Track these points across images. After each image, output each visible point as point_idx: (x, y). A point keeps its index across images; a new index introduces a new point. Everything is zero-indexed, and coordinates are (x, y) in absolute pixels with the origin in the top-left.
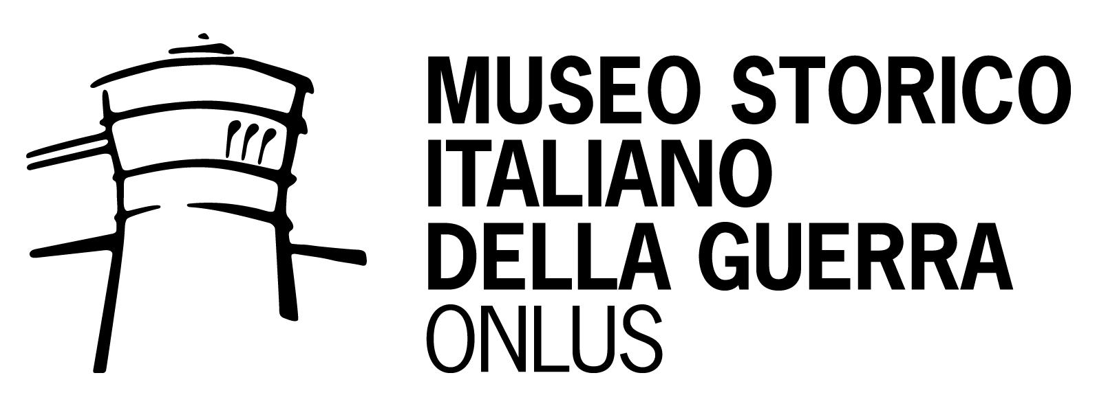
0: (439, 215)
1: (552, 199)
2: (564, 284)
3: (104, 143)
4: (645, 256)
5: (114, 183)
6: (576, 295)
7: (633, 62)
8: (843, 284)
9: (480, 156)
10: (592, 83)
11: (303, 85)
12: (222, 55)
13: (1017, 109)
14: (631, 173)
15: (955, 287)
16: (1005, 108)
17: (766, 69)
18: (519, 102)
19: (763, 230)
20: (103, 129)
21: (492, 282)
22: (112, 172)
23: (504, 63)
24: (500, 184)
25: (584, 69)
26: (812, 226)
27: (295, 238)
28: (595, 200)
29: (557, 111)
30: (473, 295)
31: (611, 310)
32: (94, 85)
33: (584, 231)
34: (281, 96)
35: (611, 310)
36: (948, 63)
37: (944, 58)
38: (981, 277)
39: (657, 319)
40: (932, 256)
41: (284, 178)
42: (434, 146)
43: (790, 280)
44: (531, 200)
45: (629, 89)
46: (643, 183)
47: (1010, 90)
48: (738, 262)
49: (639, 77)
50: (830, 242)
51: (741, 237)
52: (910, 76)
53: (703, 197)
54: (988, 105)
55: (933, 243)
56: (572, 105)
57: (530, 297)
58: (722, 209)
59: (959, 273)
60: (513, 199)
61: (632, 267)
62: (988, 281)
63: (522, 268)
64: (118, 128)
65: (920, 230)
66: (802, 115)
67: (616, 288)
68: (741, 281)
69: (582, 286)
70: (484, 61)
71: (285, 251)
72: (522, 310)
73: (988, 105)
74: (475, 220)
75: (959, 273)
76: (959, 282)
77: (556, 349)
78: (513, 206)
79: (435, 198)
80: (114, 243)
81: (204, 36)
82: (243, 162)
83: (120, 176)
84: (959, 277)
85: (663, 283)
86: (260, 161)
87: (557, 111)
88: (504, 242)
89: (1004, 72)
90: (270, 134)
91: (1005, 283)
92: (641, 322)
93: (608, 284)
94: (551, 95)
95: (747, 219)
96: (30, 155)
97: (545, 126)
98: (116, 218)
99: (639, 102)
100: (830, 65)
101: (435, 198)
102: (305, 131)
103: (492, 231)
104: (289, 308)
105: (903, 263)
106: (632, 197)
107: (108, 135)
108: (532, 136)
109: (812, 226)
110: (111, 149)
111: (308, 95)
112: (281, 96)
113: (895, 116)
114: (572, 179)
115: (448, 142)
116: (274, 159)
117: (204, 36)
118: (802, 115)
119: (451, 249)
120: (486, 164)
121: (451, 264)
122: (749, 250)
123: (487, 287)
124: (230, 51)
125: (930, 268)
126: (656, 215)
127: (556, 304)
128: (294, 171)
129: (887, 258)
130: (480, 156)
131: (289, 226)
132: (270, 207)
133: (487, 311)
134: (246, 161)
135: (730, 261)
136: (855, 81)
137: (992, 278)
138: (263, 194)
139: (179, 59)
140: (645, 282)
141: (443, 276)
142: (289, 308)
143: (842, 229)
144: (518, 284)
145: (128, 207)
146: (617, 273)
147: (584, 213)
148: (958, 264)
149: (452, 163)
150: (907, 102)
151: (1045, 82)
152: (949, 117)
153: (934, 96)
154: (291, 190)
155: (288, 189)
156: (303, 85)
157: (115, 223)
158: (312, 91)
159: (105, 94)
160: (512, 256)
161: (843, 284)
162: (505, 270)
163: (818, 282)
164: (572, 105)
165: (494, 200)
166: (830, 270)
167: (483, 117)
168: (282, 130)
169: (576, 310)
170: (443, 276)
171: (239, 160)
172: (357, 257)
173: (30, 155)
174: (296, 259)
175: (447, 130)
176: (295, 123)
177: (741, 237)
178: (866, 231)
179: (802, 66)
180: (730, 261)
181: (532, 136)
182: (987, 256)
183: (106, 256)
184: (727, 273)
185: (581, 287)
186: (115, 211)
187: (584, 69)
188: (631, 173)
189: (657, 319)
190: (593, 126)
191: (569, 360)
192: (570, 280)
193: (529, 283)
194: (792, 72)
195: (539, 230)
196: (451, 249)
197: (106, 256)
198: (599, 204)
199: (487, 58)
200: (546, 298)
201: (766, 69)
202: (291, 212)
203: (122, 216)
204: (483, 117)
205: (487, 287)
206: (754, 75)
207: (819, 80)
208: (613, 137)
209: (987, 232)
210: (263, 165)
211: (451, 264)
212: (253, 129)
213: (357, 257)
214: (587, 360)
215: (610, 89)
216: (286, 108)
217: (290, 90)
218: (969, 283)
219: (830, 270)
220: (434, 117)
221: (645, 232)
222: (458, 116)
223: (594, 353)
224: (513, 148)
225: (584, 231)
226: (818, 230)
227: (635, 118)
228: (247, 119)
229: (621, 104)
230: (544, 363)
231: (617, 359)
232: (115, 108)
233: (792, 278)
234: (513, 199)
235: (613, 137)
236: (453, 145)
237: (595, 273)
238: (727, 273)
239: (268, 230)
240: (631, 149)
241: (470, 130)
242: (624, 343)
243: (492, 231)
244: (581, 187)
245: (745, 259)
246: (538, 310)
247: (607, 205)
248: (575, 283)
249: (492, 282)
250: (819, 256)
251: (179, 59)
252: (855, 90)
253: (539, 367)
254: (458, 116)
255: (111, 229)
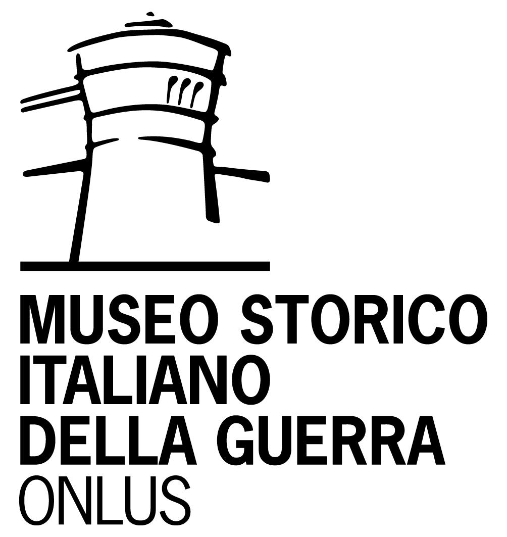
0: (29, 410)
1: (110, 399)
2: (119, 460)
3: (77, 92)
4: (178, 440)
5: (85, 122)
6: (127, 469)
7: (169, 299)
8: (322, 460)
9: (58, 367)
10: (139, 315)
11: (223, 50)
12: (163, 28)
13: (448, 333)
14: (168, 380)
15: (403, 463)
16: (439, 332)
17: (266, 304)
18: (87, 329)
19: (263, 421)
20: (76, 82)
21: (67, 459)
22: (83, 114)
23: (75, 300)
24: (73, 388)
25: (133, 304)
26: (300, 419)
27: (217, 162)
28: (141, 400)
29: (114, 335)
30: (53, 468)
31: (153, 480)
32: (70, 50)
33: (134, 422)
34: (207, 58)
35: (153, 480)
36: (398, 300)
37: (260, 418)
38: (422, 455)
39: (187, 486)
40: (386, 440)
41: (209, 118)
42: (25, 360)
43: (283, 458)
44: (95, 400)
45: (166, 319)
46: (176, 387)
47: (443, 319)
48: (246, 445)
49: (174, 310)
50: (312, 430)
51: (248, 426)
52: (371, 309)
53: (220, 398)
54: (427, 330)
55: (388, 430)
56: (125, 330)
57: (94, 470)
58: (233, 406)
59: (406, 452)
60: (82, 397)
61: (169, 448)
62: (426, 458)
63: (89, 449)
64: (88, 81)
65: (378, 421)
66: (292, 338)
67: (157, 464)
68: (248, 458)
69: (132, 462)
70: (62, 298)
71: (210, 171)
72: (89, 479)
73: (427, 330)
74: (54, 414)
75: (406, 452)
76: (406, 459)
77: (113, 508)
78: (82, 404)
79: (25, 398)
80: (84, 166)
81: (151, 14)
82: (180, 106)
83: (89, 116)
84: (406, 456)
85: (191, 460)
86: (192, 106)
87: (114, 335)
88: (76, 430)
89: (439, 306)
90: (199, 86)
91: (440, 460)
92: (175, 488)
93: (151, 460)
94: (109, 323)
95: (252, 413)
96: (23, 101)
97: (106, 345)
98: (86, 147)
99: (173, 328)
100: (313, 301)
101: (25, 398)
102: (225, 84)
103: (67, 422)
104: (213, 214)
105: (366, 445)
106: (168, 397)
107: (80, 86)
108: (96, 353)
109: (300, 419)
110: (83, 97)
111: (227, 57)
112: (207, 58)
113: (359, 338)
114: (124, 384)
115: (35, 357)
116: (201, 105)
117: (151, 14)
118: (292, 338)
119: (37, 435)
120: (62, 373)
121: (37, 446)
122: (253, 436)
123: (63, 463)
124: (170, 25)
125: (385, 449)
126: (186, 411)
127: (113, 476)
128: (216, 113)
129: (353, 442)
130: (58, 367)
131: (213, 153)
132: (199, 139)
133: (63, 480)
134: (182, 106)
135: (240, 444)
136: (330, 313)
137: (430, 456)
138: (194, 130)
139: (132, 31)
140: (177, 458)
141: (31, 455)
142: (213, 214)
143: (321, 420)
144: (85, 460)
145: (95, 139)
146: (157, 453)
147: (134, 409)
148: (405, 446)
149: (37, 372)
150: (368, 328)
151: (468, 313)
152: (398, 339)
153: (388, 324)
154: (215, 127)
155: (213, 126)
156: (223, 50)
157: (85, 151)
158: (230, 54)
159: (78, 57)
160: (82, 440)
161: (322, 460)
162: (76, 450)
163: (303, 459)
164: (125, 330)
165: (68, 399)
166: (312, 450)
167: (60, 339)
168: (208, 83)
169: (128, 480)
170: (31, 455)
171: (177, 105)
172: (263, 176)
173: (23, 101)
174: (218, 178)
175: (34, 348)
176: (217, 78)
177: (248, 426)
178: (339, 422)
179: (292, 302)
180: (240, 444)
181: (96, 353)
182: (426, 440)
183: (79, 175)
184: (237, 453)
185: (131, 463)
186: (85, 143)
187: (133, 304)
188: (168, 380)
189: (187, 486)
190: (140, 346)
191: (123, 516)
192: (123, 458)
193: (94, 460)
194: (284, 307)
195: (101, 421)
196: (37, 435)
197: (79, 175)
198: (145, 403)
199: (63, 296)
200: (107, 471)
201: (266, 304)
202: (214, 143)
203: (91, 146)
204: (60, 339)
205: (63, 463)
206: (257, 308)
207: (304, 312)
208: (154, 354)
209: (426, 423)
210: (194, 108)
211: (37, 446)
212: (187, 82)
213: (263, 176)
214: (136, 516)
215: (152, 319)
216: (210, 66)
217: (213, 53)
218: (413, 460)
219: (312, 450)
220: (25, 339)
221: (177, 423)
222: (42, 338)
223: (140, 511)
224: (82, 362)
225: (134, 422)
226: (304, 421)
227: (170, 339)
228: (182, 75)
229: (160, 329)
230: (104, 518)
231: (158, 515)
232: (86, 67)
233: (284, 457)
234: (82, 397)
235: (154, 354)
236: (38, 360)
237: (142, 453)
238: (237, 453)
239: (198, 156)
240: (168, 362)
241: (51, 348)
242: (162, 503)
243: (67, 422)
244: (131, 390)
245: (251, 443)
246: (100, 479)
247: (150, 403)
248: (127, 460)
249: (67, 459)
250: (305, 442)
251: (132, 31)
252: (330, 319)
253: (101, 521)
254: (42, 338)
255: (83, 155)
